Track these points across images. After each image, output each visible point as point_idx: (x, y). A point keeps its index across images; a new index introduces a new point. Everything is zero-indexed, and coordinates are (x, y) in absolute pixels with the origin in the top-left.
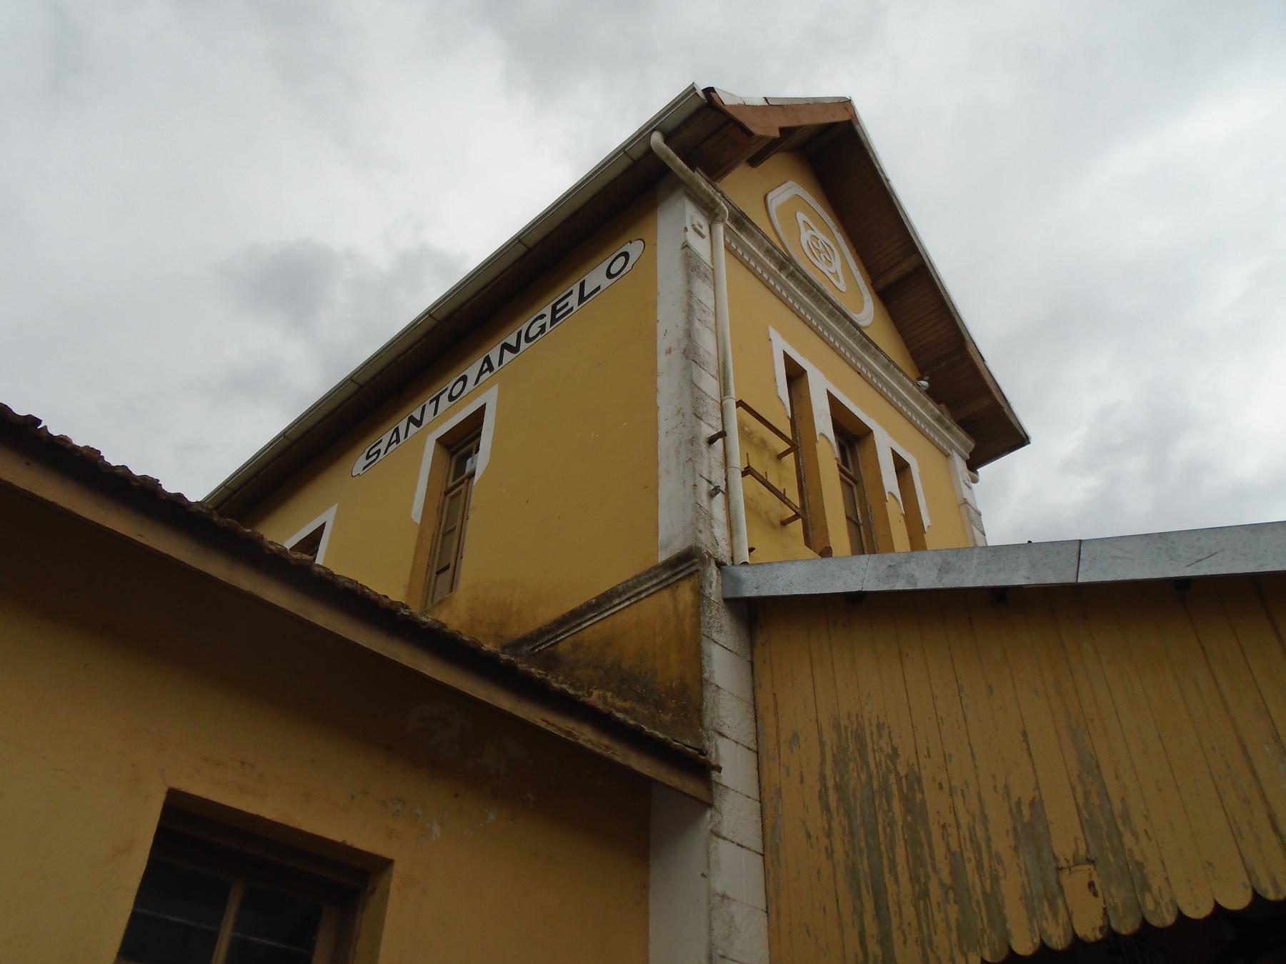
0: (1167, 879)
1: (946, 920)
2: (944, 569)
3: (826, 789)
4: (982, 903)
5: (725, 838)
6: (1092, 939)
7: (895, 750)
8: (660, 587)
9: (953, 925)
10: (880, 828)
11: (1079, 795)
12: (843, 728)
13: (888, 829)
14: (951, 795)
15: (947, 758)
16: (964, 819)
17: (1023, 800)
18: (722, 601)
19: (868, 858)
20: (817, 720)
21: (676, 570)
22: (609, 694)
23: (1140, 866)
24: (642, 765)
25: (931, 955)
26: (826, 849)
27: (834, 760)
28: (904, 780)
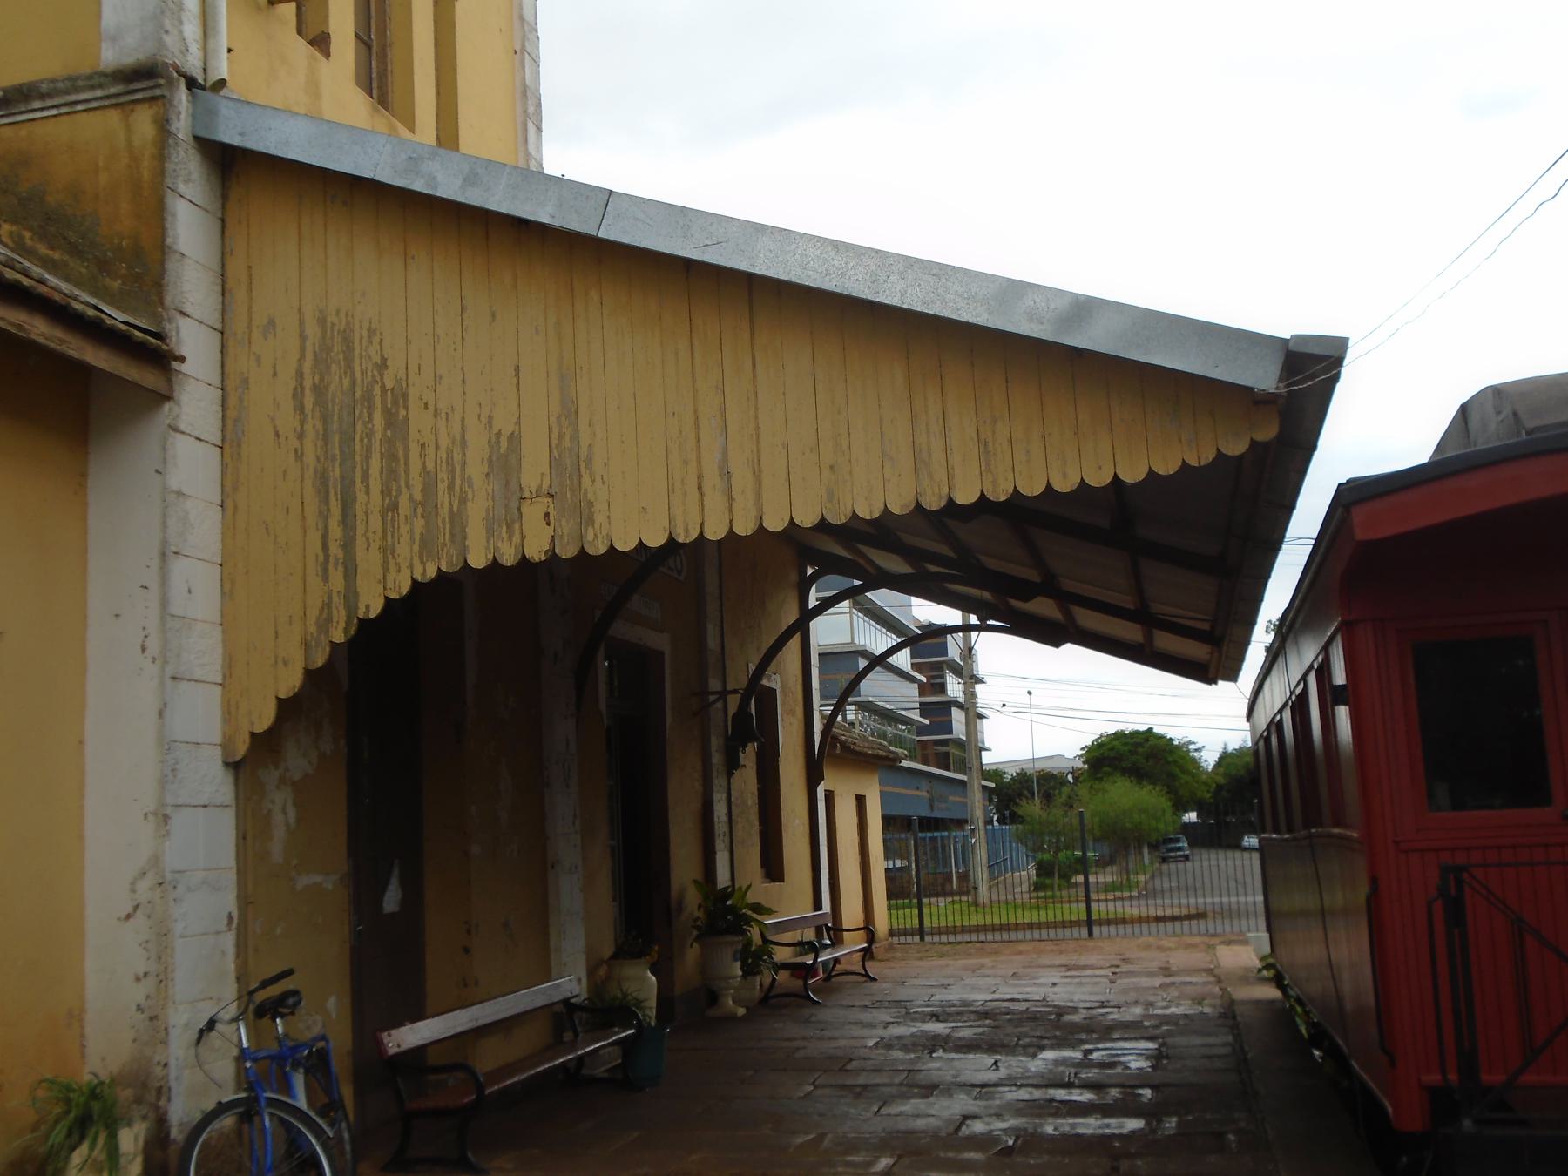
0: (609, 517)
1: (412, 531)
2: (471, 180)
3: (302, 388)
4: (447, 520)
5: (183, 433)
6: (537, 560)
7: (384, 360)
8: (107, 102)
9: (417, 537)
10: (358, 437)
11: (555, 435)
12: (329, 324)
13: (366, 440)
14: (435, 416)
15: (437, 378)
16: (444, 441)
17: (502, 432)
18: (191, 138)
19: (340, 465)
20: (299, 310)
21: (132, 87)
22: (27, 234)
23: (591, 504)
24: (98, 357)
25: (391, 561)
26: (296, 450)
27: (354, 440)
28: (389, 392)
